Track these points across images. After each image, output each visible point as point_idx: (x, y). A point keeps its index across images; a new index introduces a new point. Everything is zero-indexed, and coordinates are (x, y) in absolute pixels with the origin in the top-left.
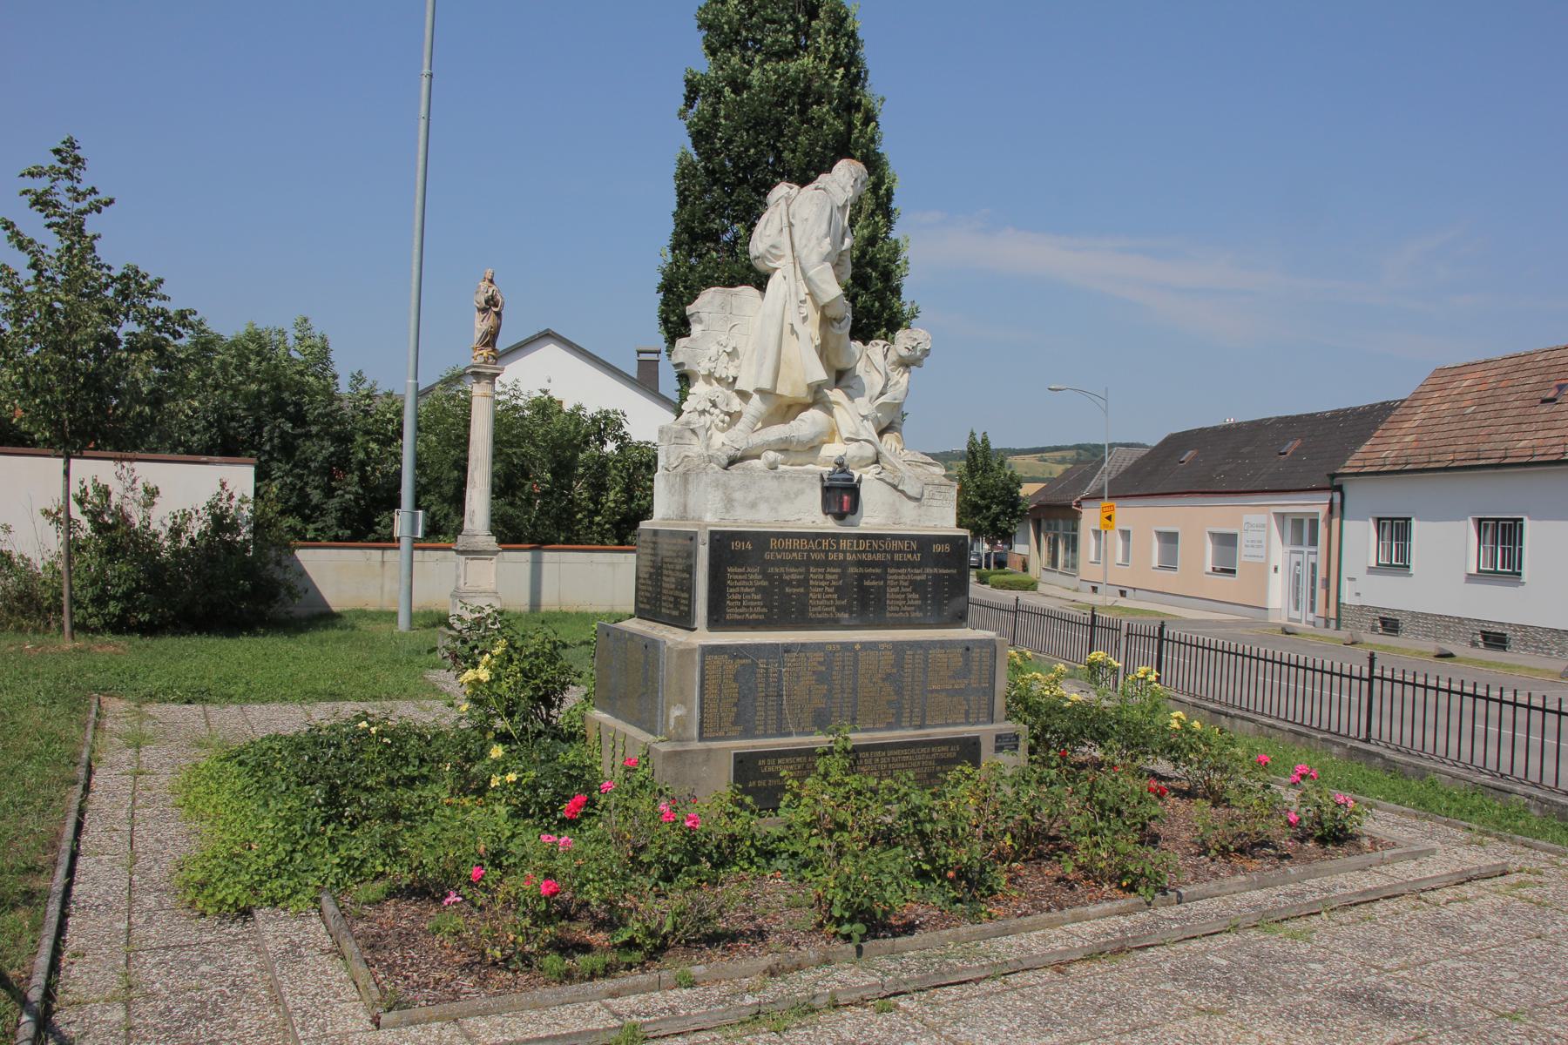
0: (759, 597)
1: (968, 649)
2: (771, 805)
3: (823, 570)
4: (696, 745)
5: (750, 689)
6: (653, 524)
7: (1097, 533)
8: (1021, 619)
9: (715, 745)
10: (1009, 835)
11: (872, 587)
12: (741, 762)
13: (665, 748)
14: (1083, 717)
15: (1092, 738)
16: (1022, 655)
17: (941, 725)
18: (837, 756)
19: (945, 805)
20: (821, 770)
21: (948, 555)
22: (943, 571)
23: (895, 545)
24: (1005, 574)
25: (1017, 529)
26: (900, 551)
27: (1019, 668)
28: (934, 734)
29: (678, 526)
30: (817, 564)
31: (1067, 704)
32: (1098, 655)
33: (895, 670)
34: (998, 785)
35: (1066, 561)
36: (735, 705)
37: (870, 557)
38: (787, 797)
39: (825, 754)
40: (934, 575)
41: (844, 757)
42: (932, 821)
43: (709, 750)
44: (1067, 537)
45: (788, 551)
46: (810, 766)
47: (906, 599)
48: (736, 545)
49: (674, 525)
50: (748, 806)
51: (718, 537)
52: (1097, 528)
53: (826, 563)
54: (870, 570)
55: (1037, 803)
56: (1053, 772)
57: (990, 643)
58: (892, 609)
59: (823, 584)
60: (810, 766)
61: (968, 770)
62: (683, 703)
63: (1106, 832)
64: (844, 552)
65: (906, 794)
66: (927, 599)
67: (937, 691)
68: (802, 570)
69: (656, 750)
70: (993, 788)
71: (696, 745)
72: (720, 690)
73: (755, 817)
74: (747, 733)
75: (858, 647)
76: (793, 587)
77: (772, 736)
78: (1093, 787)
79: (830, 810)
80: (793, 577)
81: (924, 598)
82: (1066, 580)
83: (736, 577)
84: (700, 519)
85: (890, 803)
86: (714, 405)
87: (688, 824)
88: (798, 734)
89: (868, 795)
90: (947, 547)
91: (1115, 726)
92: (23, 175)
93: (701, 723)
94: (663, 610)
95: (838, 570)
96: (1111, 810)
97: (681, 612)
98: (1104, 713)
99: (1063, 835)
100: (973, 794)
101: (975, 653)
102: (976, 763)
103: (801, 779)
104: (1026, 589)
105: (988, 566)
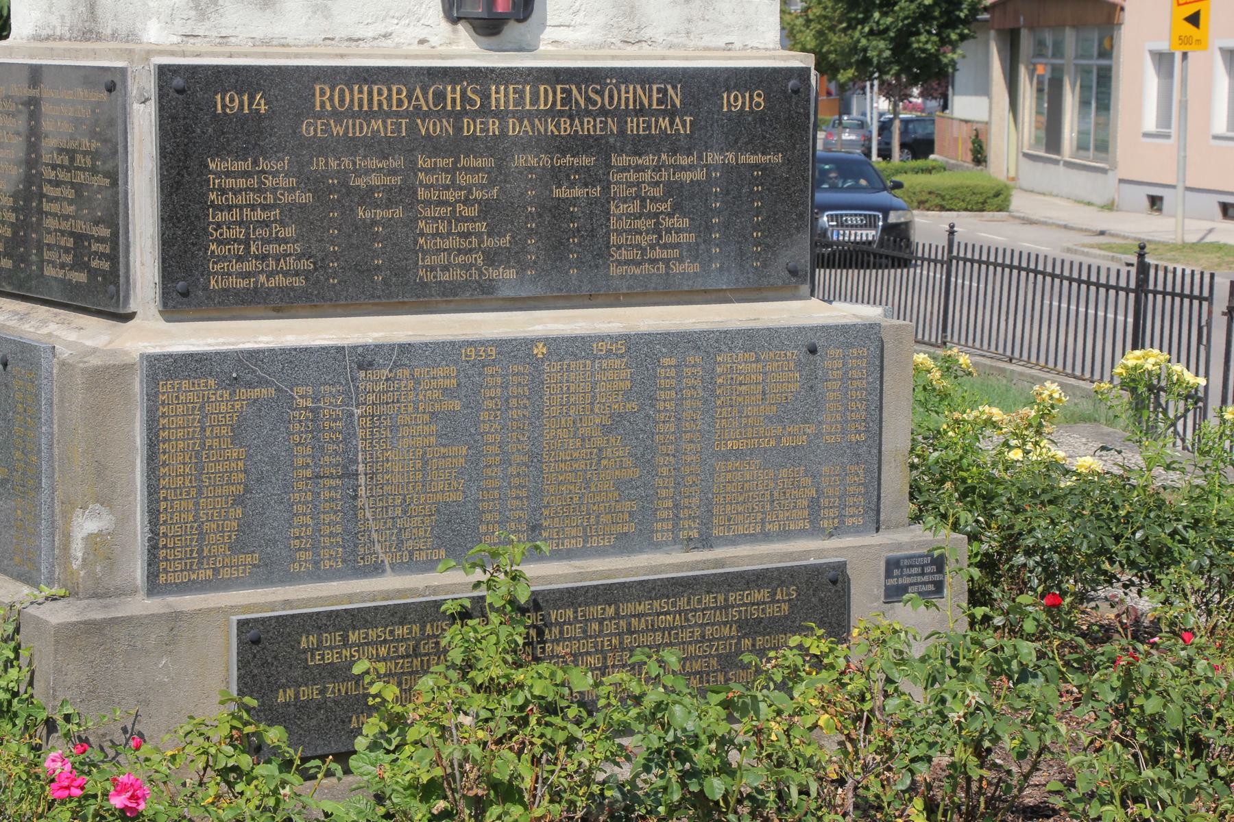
0: (290, 232)
1: (813, 351)
2: (335, 748)
4: (142, 605)
6: (10, 51)
7: (1163, 60)
8: (963, 279)
9: (188, 602)
10: (918, 803)
11: (574, 201)
12: (256, 642)
13: (59, 615)
14: (1105, 510)
15: (1132, 564)
16: (949, 367)
17: (752, 538)
18: (494, 618)
19: (758, 732)
20: (456, 656)
21: (761, 118)
23: (628, 94)
24: (929, 171)
25: (961, 57)
26: (640, 111)
27: (944, 396)
28: (734, 560)
29: (76, 53)
30: (434, 146)
31: (1066, 483)
32: (1150, 359)
34: (889, 681)
35: (1083, 134)
36: (239, 501)
38: (373, 726)
39: (465, 615)
40: (727, 169)
41: (512, 622)
42: (726, 770)
43: (176, 617)
44: (1086, 71)
45: (359, 114)
46: (429, 647)
47: (657, 230)
48: (229, 103)
49: (67, 53)
50: (275, 751)
51: (178, 82)
52: (1163, 46)
53: (458, 146)
55: (985, 722)
56: (1028, 650)
57: (869, 333)
58: (625, 254)
59: (450, 196)
60: (429, 647)
61: (817, 646)
62: (105, 501)
63: (1163, 792)
64: (501, 115)
65: (659, 706)
66: (709, 228)
67: (739, 454)
68: (396, 162)
69: (38, 621)
70: (878, 687)
71: (142, 605)
73: (293, 778)
74: (269, 573)
75: (540, 350)
77: (334, 575)
78: (1128, 680)
79: (475, 751)
80: (375, 180)
81: (703, 228)
82: (1081, 183)
83: (230, 182)
84: (131, 36)
85: (626, 730)
87: (117, 802)
88: (398, 568)
89: (572, 712)
91: (1191, 535)
93: (153, 549)
94: (49, 271)
96: (1178, 738)
97: (93, 273)
98: (1160, 505)
99: (1058, 802)
100: (827, 703)
101: (831, 360)
102: (838, 629)
103: (405, 680)
104: (981, 207)
105: (885, 154)
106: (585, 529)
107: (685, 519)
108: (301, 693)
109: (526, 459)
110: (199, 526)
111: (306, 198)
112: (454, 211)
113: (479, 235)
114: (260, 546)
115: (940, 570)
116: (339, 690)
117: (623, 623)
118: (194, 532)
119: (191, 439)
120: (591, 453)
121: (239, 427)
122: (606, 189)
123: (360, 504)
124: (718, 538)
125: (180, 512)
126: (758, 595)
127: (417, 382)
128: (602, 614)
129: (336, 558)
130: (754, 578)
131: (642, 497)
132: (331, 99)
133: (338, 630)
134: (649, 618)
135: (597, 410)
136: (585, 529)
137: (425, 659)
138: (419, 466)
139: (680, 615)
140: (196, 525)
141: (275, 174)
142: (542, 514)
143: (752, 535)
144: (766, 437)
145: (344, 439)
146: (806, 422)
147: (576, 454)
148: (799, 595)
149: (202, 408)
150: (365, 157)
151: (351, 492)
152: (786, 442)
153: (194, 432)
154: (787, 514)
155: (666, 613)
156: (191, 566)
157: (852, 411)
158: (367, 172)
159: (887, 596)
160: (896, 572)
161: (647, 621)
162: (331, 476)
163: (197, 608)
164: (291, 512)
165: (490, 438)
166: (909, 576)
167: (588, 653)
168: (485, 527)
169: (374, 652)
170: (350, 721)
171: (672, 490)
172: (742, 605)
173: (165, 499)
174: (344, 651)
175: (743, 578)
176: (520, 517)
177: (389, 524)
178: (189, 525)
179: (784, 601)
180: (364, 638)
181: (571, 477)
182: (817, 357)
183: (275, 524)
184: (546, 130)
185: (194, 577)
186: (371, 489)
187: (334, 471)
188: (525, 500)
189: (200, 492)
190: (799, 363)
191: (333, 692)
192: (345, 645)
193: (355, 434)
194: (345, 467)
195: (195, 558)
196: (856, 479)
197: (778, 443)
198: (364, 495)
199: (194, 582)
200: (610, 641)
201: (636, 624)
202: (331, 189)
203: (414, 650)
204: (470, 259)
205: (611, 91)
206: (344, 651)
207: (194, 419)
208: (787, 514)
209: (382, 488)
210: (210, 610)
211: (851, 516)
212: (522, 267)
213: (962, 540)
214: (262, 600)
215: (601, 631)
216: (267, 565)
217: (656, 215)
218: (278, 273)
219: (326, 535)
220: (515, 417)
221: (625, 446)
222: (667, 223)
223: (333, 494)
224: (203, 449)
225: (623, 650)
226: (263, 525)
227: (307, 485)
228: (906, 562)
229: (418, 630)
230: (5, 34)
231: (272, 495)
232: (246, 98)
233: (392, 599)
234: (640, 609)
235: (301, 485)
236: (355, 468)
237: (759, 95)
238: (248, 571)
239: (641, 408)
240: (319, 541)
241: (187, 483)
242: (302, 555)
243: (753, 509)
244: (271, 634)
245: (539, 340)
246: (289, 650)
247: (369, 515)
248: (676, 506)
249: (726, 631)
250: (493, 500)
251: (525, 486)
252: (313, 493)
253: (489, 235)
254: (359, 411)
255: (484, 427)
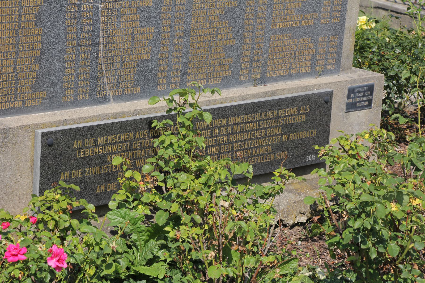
12: (50, 145)
36: (37, 60)
67: (282, 30)
77: (86, 103)
106: (208, 74)
107: (255, 67)
108: (73, 174)
109: (182, 34)
110: (16, 75)
114: (47, 87)
116: (92, 172)
117: (229, 129)
118: (13, 79)
119: (14, 22)
120: (213, 31)
121: (39, 15)
123: (100, 61)
124: (268, 78)
125: (6, 67)
126: (293, 111)
128: (221, 124)
129: (86, 93)
130: (291, 101)
131: (236, 56)
133: (93, 137)
134: (242, 125)
135: (218, 6)
136: (208, 74)
137: (135, 152)
138: (130, 39)
139: (256, 123)
140: (14, 74)
142: (188, 66)
143: (284, 76)
144: (295, 21)
145: (93, 23)
146: (314, 12)
147: (206, 32)
148: (310, 110)
151: (95, 54)
152: (304, 23)
153: (15, 17)
154: (301, 64)
155: (250, 122)
156: (11, 99)
157: (336, 5)
159: (347, 109)
160: (352, 95)
161: (241, 127)
162: (85, 45)
163: (19, 125)
164: (64, 66)
165: (166, 22)
166: (358, 97)
167: (213, 146)
168: (160, 74)
169: (110, 149)
170: (96, 189)
171: (250, 51)
172: (284, 117)
174: (95, 149)
175: (286, 101)
176: (177, 68)
177: (113, 73)
178: (10, 75)
179: (304, 114)
180: (106, 141)
181: (203, 45)
183: (56, 74)
185: (12, 105)
186: (105, 53)
187: (87, 42)
188: (180, 58)
189: (17, 55)
191: (89, 173)
192: (96, 146)
193: (99, 20)
194: (93, 40)
195: (13, 94)
196: (334, 44)
197: (300, 24)
198: (102, 56)
199: (12, 109)
200: (223, 138)
201: (236, 129)
203: (130, 147)
206: (95, 149)
207: (15, 10)
208: (301, 64)
209: (111, 52)
210: (25, 126)
211: (330, 64)
213: (382, 77)
214: (51, 120)
215: (219, 133)
216: (50, 98)
219: (82, 80)
220: (179, 10)
221: (230, 27)
223: (86, 56)
224: (20, 28)
225: (229, 143)
226: (49, 74)
227: (73, 50)
228: (357, 90)
229: (132, 135)
231: (55, 56)
233: (118, 117)
234: (238, 120)
235: (70, 50)
236: (98, 40)
238: (40, 101)
239: (239, 5)
240: (78, 83)
241: (11, 49)
242: (69, 92)
243: (286, 61)
244: (59, 141)
246: (68, 149)
247: (103, 68)
248: (251, 60)
249: (276, 131)
250: (165, 58)
251: (181, 50)
252: (76, 55)
254: (102, 6)
255: (163, 16)
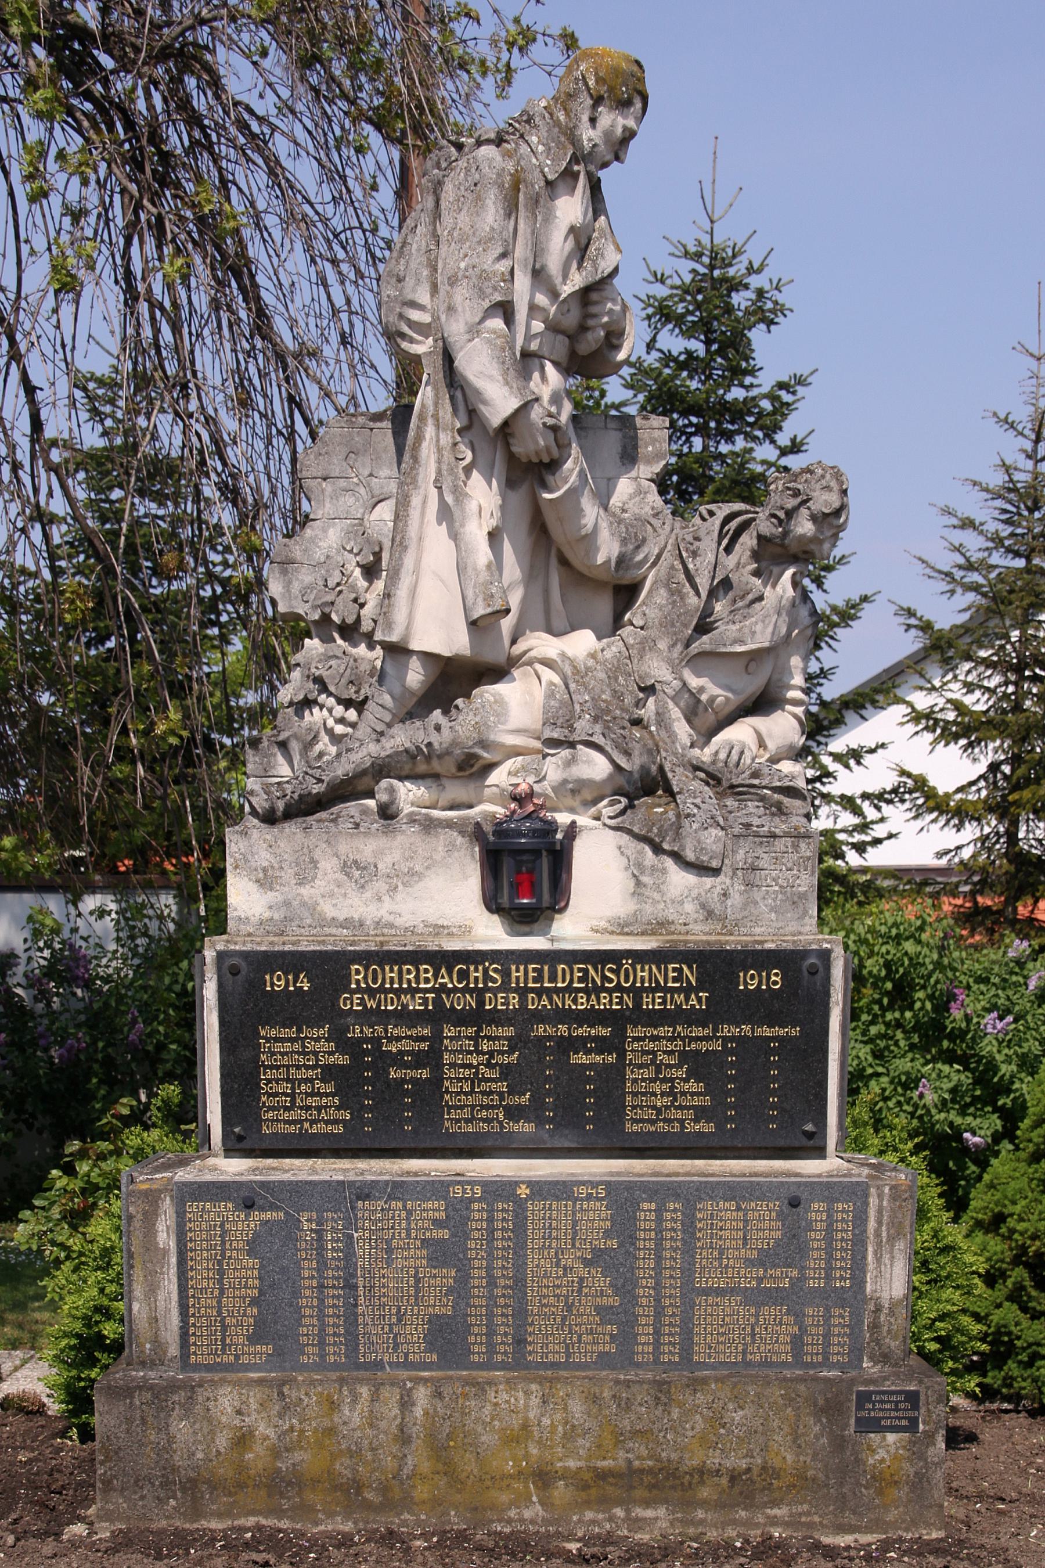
1: (794, 1203)
3: (471, 1031)
5: (284, 1270)
22: (767, 1032)
30: (462, 1019)
33: (614, 1243)
36: (254, 1302)
37: (582, 1004)
40: (741, 1040)
47: (671, 1093)
48: (277, 982)
54: (583, 1031)
64: (523, 992)
72: (221, 1272)
76: (406, 1066)
86: (324, 689)
90: (776, 977)
92: (865, 599)
95: (509, 1031)
106: (567, 1346)
111: (342, 1060)
112: (477, 1073)
113: (501, 1094)
115: (915, 1407)
122: (622, 1054)
127: (410, 1213)
132: (365, 978)
135: (578, 1245)
141: (318, 1040)
149: (222, 1226)
150: (395, 1026)
158: (399, 1039)
162: (334, 1287)
166: (880, 1410)
173: (193, 1296)
181: (552, 1300)
182: (800, 1209)
184: (564, 1004)
190: (780, 1215)
202: (366, 1052)
204: (491, 1114)
205: (627, 970)
212: (540, 1121)
217: (672, 1080)
218: (319, 1121)
222: (679, 1087)
226: (276, 1323)
230: (563, 904)
232: (290, 977)
237: (776, 975)
242: (310, 1350)
245: (523, 1182)
253: (509, 1093)
